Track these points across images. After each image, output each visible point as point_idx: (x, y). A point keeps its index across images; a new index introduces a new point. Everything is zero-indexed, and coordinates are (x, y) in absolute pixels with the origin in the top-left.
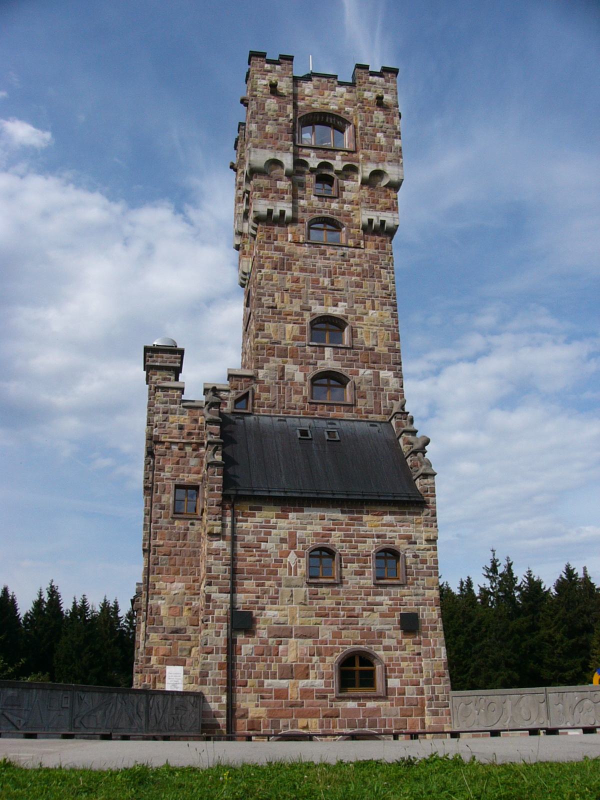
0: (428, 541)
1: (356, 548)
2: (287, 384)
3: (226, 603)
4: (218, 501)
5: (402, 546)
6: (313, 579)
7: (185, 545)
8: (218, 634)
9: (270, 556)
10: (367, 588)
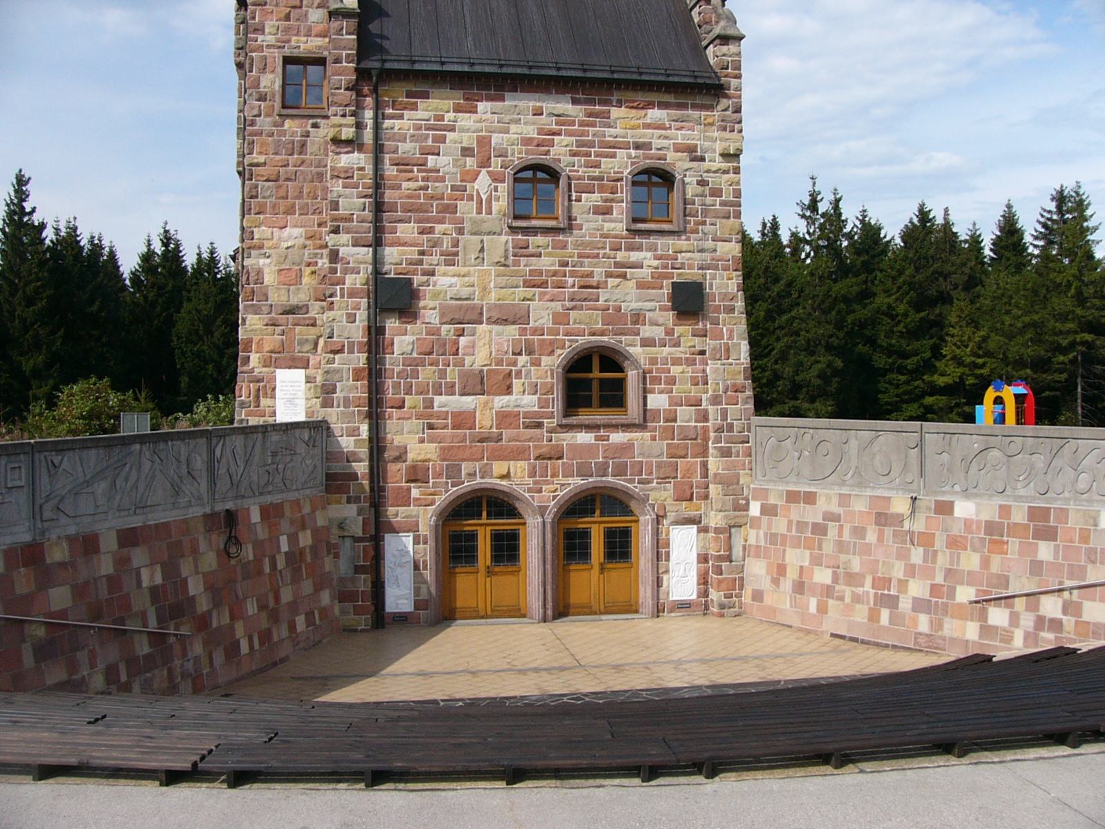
0: (726, 156)
1: (598, 166)
3: (365, 263)
4: (349, 82)
5: (679, 164)
6: (520, 219)
7: (303, 162)
8: (352, 319)
9: (443, 180)
10: (616, 237)
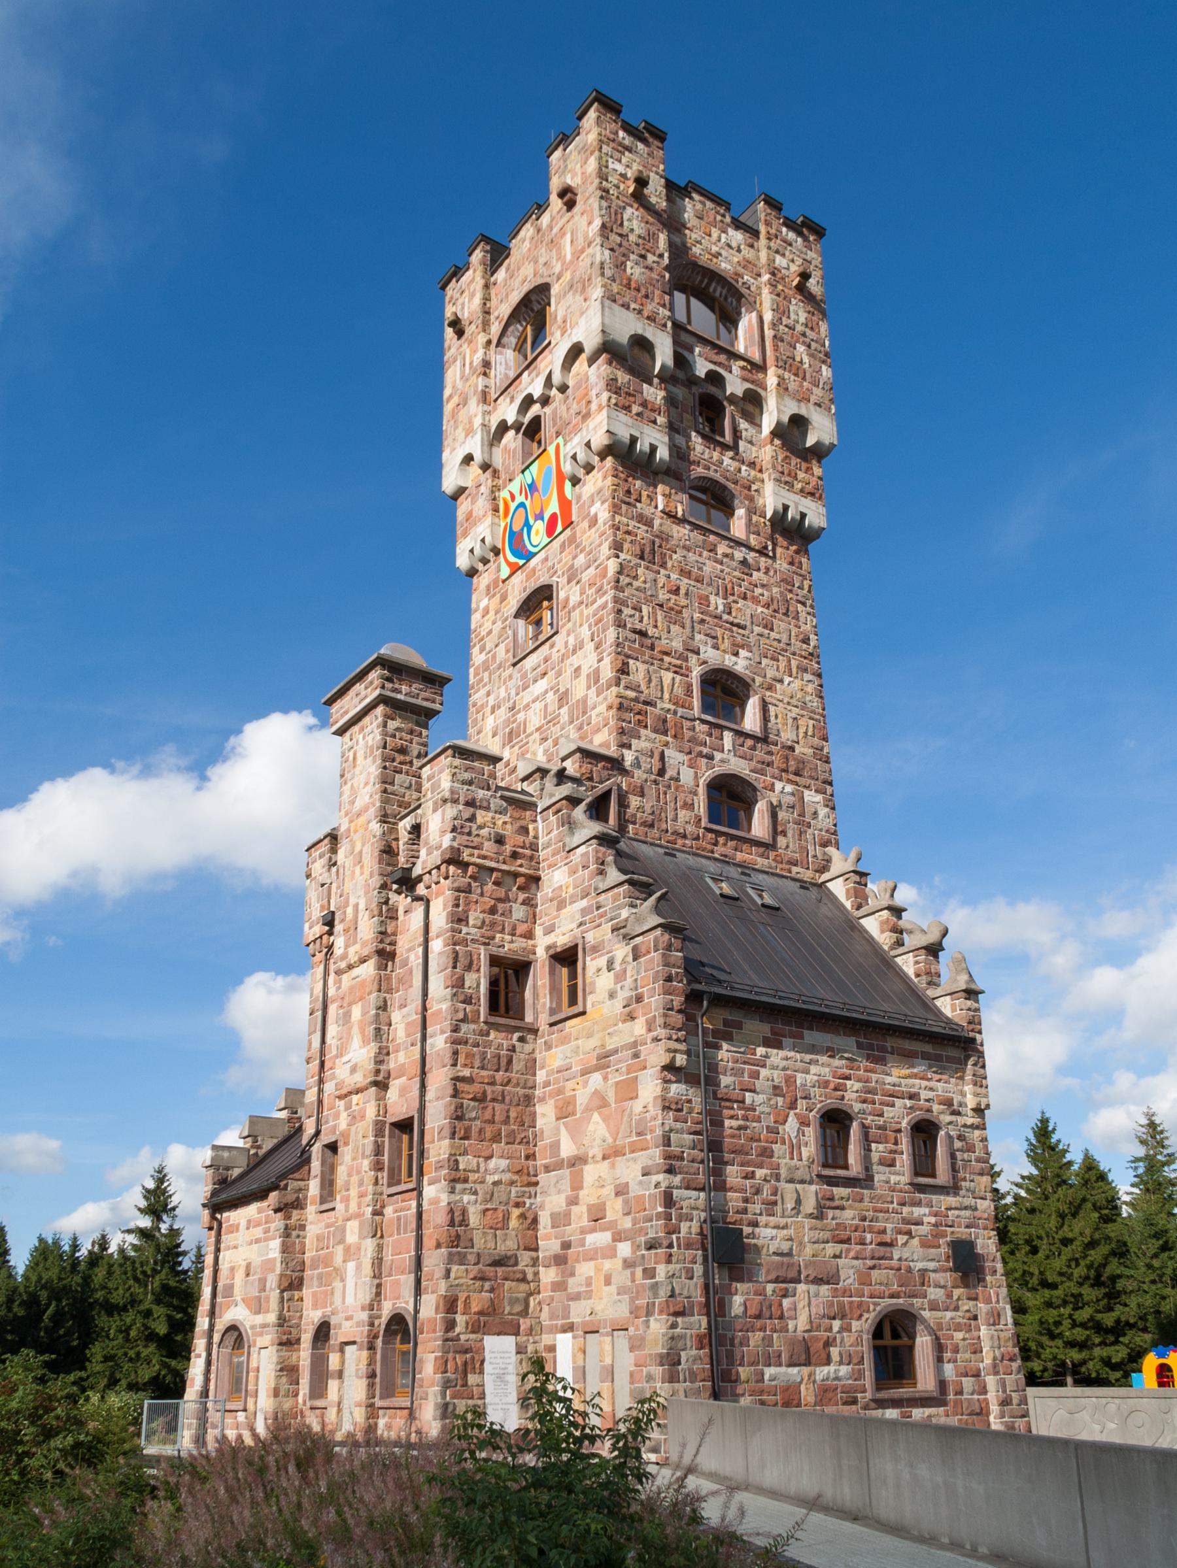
1: (881, 1115)
2: (669, 787)
3: (697, 1209)
5: (942, 1117)
7: (509, 1081)
